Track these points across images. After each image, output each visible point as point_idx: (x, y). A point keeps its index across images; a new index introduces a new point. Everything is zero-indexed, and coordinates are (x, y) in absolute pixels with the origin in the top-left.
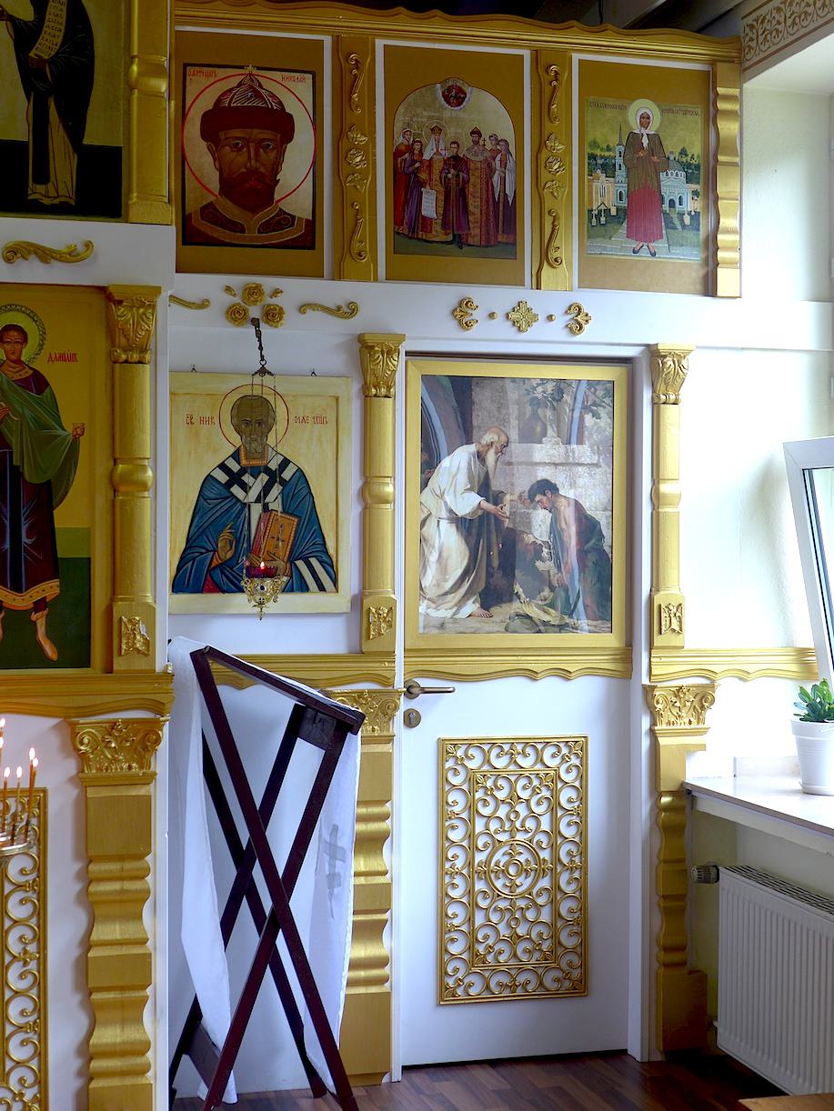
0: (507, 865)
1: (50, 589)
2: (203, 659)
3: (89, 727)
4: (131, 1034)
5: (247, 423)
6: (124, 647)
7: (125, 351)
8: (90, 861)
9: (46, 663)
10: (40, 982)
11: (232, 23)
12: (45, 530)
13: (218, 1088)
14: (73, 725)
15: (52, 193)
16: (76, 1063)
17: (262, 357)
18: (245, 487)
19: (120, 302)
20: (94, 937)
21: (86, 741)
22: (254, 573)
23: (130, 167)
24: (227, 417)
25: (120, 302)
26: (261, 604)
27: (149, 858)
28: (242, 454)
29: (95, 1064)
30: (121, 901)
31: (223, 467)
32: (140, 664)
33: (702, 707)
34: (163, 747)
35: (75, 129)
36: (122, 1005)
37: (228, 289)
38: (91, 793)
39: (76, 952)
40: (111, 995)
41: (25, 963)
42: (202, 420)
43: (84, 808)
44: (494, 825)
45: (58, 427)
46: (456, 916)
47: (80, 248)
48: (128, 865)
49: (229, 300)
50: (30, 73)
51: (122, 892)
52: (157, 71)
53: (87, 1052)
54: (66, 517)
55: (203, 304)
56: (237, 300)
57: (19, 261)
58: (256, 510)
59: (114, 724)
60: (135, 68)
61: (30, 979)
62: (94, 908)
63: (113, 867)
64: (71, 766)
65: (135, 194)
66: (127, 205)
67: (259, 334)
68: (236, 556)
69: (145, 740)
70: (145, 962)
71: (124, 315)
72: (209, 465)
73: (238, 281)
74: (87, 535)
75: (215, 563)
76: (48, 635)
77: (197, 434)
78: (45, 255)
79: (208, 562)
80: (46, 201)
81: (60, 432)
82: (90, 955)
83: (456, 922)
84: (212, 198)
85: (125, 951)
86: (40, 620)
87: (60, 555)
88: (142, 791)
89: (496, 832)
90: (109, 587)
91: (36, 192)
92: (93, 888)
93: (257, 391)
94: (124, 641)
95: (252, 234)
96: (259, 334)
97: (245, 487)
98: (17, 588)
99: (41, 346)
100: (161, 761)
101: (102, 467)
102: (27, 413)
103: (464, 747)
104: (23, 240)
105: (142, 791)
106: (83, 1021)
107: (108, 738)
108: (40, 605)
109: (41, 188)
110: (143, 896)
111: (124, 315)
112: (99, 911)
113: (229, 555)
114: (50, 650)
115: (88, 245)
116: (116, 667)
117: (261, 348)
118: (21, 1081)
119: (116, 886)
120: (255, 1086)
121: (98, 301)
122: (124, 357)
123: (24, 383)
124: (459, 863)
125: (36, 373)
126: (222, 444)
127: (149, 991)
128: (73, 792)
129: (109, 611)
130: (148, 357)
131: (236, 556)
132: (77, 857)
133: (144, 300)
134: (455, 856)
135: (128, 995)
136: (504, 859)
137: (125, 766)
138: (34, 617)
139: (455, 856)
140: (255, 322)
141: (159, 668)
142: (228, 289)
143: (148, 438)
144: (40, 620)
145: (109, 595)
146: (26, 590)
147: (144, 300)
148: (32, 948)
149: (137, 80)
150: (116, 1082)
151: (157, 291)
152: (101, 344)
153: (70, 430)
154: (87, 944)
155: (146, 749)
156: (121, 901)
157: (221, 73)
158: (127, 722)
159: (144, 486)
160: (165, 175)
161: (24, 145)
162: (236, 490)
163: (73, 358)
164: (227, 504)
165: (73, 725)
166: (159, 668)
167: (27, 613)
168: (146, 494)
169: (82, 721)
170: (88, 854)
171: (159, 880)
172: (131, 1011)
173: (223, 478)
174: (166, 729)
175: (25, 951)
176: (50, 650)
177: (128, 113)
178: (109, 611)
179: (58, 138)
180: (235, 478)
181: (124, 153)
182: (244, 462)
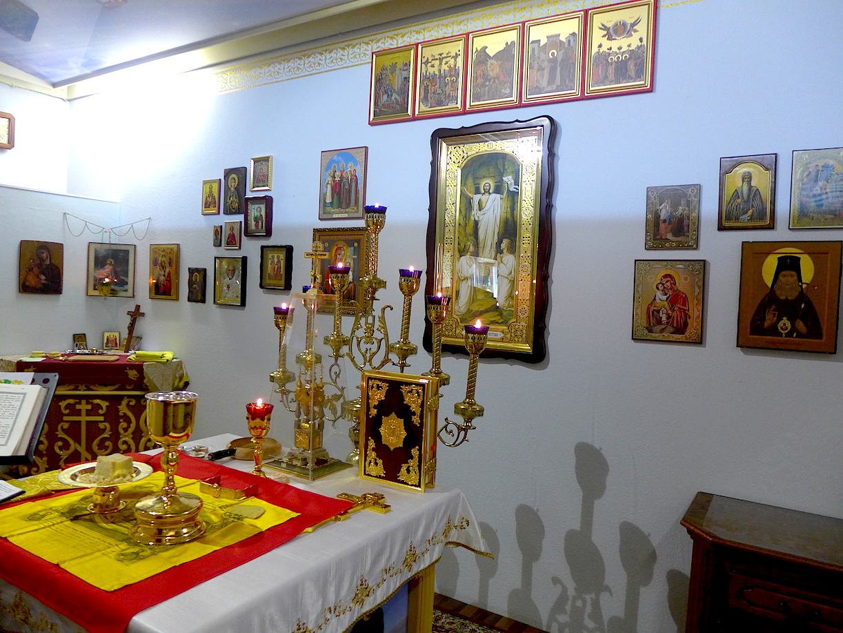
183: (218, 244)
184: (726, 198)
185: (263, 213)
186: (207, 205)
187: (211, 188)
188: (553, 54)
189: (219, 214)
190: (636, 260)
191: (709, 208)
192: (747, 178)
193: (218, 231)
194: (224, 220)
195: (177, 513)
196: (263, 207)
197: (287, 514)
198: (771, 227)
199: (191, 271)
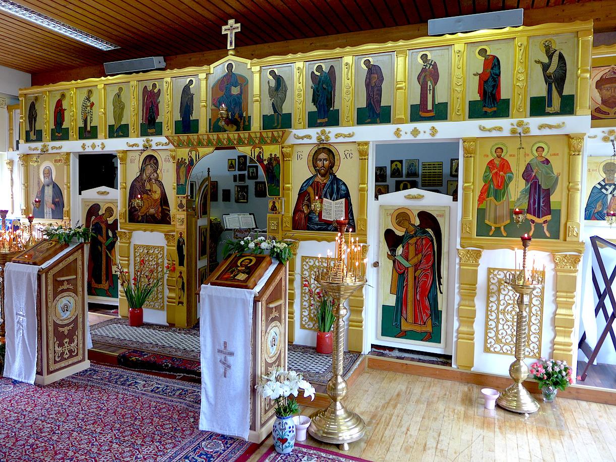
0: (511, 311)
1: (548, 218)
2: (594, 239)
3: (558, 256)
4: (566, 340)
5: (608, 171)
6: (570, 234)
7: (574, 152)
8: (557, 292)
9: (547, 238)
10: (541, 322)
11: (607, 53)
12: (548, 202)
13: (591, 361)
14: (554, 255)
15: (553, 109)
16: (550, 345)
17: (615, 151)
18: (607, 190)
19: (573, 138)
20: (557, 312)
21: (557, 259)
22: (608, 215)
23: (577, 100)
24: (601, 169)
25: (573, 138)
26: (611, 224)
27: (575, 293)
28: (606, 179)
29: (555, 346)
30: (566, 304)
31: (599, 184)
32: (575, 239)
33: (575, 263)
34: (581, 264)
35: (560, 92)
36: (565, 332)
37: (603, 132)
38: (558, 273)
39: (552, 315)
40: (562, 329)
41: (537, 316)
42: (593, 170)
43: (556, 277)
44: (507, 298)
45: (551, 173)
46: (491, 325)
47: (561, 124)
48: (569, 294)
49: (604, 135)
50: (547, 78)
51: (567, 301)
52: (586, 71)
53: (553, 343)
54: (553, 198)
55: (595, 137)
56: (606, 135)
57: (543, 129)
58: (610, 196)
59: (566, 255)
60: (579, 71)
61: (538, 321)
62: (557, 305)
63: (564, 294)
64: (553, 266)
65: (578, 108)
66: (576, 111)
67: (613, 145)
68: (603, 209)
69: (575, 260)
70: (572, 321)
71: (574, 142)
72: (595, 183)
73: (606, 129)
74: (560, 203)
75: (595, 211)
76: (547, 230)
77: (591, 174)
78: (550, 127)
79: (593, 211)
80: (551, 112)
81: (553, 175)
82: (556, 317)
83: (491, 327)
84: (599, 106)
85: (566, 317)
86: (545, 226)
87: (551, 209)
88: (574, 274)
89: (508, 300)
90: (566, 217)
91: (548, 110)
92: (557, 299)
93: (612, 161)
94: (570, 233)
95: (612, 115)
96: (613, 145)
97: (607, 190)
98: (539, 217)
99: (548, 152)
100: (580, 266)
101: (565, 184)
102: (543, 170)
103: (497, 271)
104: (544, 123)
105: (574, 274)
106: (553, 335)
107: (564, 259)
108: (545, 222)
109: (549, 109)
110: (573, 303)
111: (574, 142)
112: (559, 305)
113: (600, 209)
114: (548, 234)
115: (563, 123)
116: (567, 240)
117: (614, 148)
118: (534, 347)
119: (565, 299)
120: (602, 362)
121: (566, 138)
122: (573, 153)
123: (543, 162)
124: (494, 308)
125: (547, 160)
126: (600, 176)
127: (573, 329)
128: (553, 273)
129: (566, 224)
130: (581, 153)
131: (603, 209)
132: (553, 290)
133: (580, 137)
134: (492, 306)
135: (566, 329)
136: (510, 309)
137: (569, 267)
138: (543, 225)
139: (492, 306)
140: (612, 141)
141: (580, 241)
142: (603, 132)
143: (579, 176)
144: (545, 226)
145: (566, 220)
146: (169, 207)
147: (580, 137)
148: (539, 313)
149: (580, 75)
150: (562, 352)
151: (585, 134)
152: (566, 150)
153: (556, 174)
154: (555, 314)
155: (575, 263)
156: (566, 304)
157: (603, 68)
158: (570, 255)
159: (578, 190)
160: (588, 100)
161: (545, 97)
162: (603, 190)
163: (558, 154)
164: (599, 195)
165: (554, 255)
166: (580, 241)
167: (542, 224)
168: (579, 192)
169: (557, 254)
170: (556, 290)
171: (577, 299)
172: (568, 334)
173: (599, 187)
174: (582, 257)
175: (537, 313)
176: (548, 234)
177: (577, 84)
178: (566, 224)
179: (555, 94)
180: (603, 187)
181: (575, 96)
182: (606, 182)
183: (235, 180)
184: (392, 170)
185: (255, 171)
186: (230, 167)
187: (232, 162)
188: (48, 173)
189: (235, 170)
190: (448, 181)
191: (389, 172)
192: (396, 165)
193: (235, 177)
194: (237, 173)
195: (57, 242)
196: (255, 169)
197: (609, 276)
198: (402, 177)
199: (224, 191)
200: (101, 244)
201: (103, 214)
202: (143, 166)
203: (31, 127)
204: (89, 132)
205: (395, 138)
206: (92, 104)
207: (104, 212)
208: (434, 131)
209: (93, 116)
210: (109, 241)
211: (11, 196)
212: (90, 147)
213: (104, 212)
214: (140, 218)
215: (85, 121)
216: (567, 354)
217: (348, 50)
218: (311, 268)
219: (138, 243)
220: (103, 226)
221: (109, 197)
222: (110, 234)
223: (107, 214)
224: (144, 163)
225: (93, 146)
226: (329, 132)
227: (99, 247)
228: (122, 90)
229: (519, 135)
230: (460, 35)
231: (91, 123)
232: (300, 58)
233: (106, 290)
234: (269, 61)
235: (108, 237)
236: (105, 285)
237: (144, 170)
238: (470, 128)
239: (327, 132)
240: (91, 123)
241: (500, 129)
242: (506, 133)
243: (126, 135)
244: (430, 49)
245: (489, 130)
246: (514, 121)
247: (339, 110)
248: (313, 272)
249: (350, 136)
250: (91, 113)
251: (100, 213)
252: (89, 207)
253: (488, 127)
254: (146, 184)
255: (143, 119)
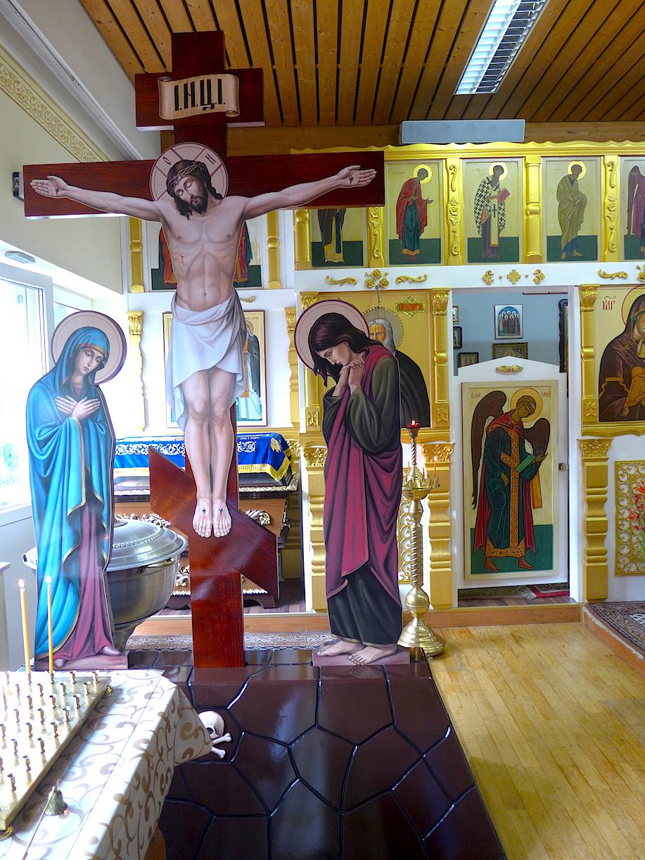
110: (605, 500)
200: (507, 469)
201: (512, 412)
202: (634, 315)
203: (327, 238)
204: (494, 248)
205: (482, 285)
206: (505, 194)
207: (515, 407)
208: (539, 276)
209: (507, 217)
210: (527, 462)
211: (141, 392)
212: (504, 278)
213: (515, 407)
214: (626, 412)
215: (485, 227)
216: (25, 593)
217: (628, 145)
218: (632, 479)
219: (622, 457)
220: (513, 434)
221: (523, 377)
222: (529, 448)
223: (522, 410)
224: (634, 309)
225: (514, 276)
226: (386, 274)
227: (503, 476)
228: (503, 171)
229: (378, 289)
230: (453, 146)
231: (499, 231)
232: (613, 148)
233: (519, 559)
234: (570, 149)
235: (523, 455)
236: (517, 548)
237: (635, 322)
238: (469, 275)
239: (638, 271)
240: (499, 231)
241: (352, 281)
242: (360, 287)
243: (593, 257)
244: (584, 158)
245: (611, 277)
246: (370, 271)
247: (518, 237)
248: (634, 486)
249: (420, 281)
250: (501, 212)
251: (506, 409)
252: (480, 399)
253: (609, 273)
254: (639, 348)
255: (629, 228)
